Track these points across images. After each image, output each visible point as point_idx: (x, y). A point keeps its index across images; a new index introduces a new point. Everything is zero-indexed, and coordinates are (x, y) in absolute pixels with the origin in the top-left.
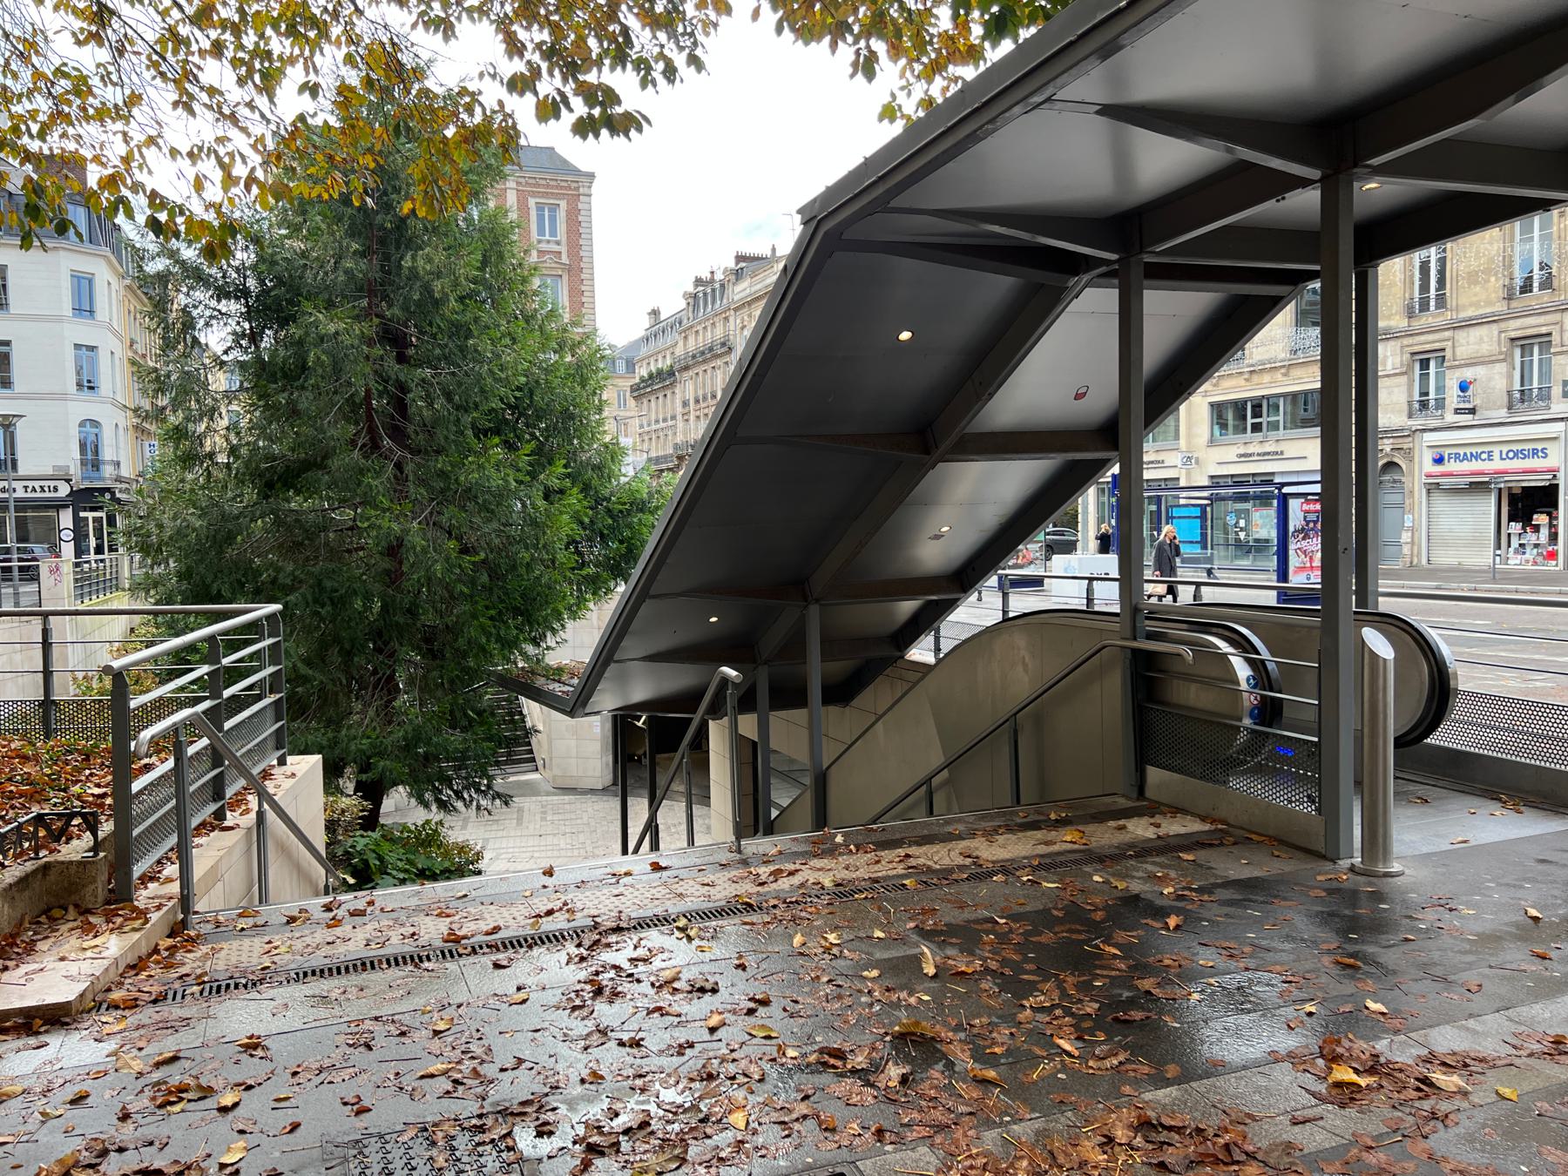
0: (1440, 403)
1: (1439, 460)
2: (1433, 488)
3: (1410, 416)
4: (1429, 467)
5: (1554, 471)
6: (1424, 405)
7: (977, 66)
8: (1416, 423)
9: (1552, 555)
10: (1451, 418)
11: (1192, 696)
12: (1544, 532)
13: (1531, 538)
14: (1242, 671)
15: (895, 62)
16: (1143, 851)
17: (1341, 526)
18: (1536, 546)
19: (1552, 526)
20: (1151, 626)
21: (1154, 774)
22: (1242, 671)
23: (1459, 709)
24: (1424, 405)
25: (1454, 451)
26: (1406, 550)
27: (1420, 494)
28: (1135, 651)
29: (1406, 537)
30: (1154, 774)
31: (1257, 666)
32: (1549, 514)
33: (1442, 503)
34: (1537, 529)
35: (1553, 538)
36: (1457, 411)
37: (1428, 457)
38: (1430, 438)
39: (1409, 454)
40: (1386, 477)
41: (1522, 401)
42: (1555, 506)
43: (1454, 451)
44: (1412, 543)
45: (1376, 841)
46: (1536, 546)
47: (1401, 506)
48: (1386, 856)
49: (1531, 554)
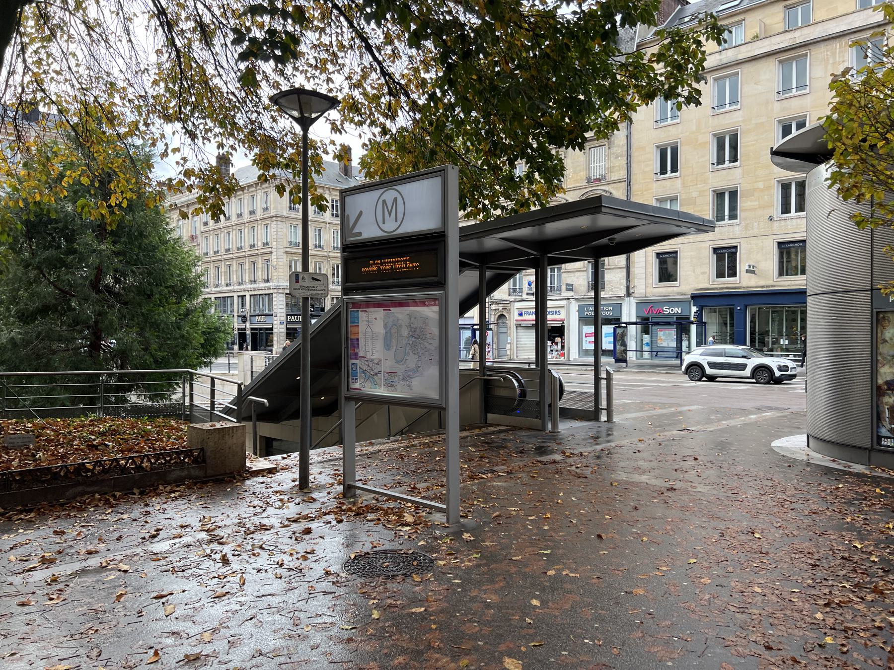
0: (521, 290)
1: (521, 315)
2: (518, 326)
3: (509, 295)
4: (517, 317)
5: (563, 320)
6: (514, 290)
7: (464, 211)
8: (512, 298)
9: (563, 355)
10: (525, 297)
11: (503, 393)
12: (560, 345)
13: (555, 347)
14: (516, 384)
15: (341, 145)
16: (493, 433)
17: (734, 351)
18: (557, 351)
19: (562, 343)
20: (488, 373)
21: (489, 415)
22: (516, 384)
23: (565, 396)
24: (514, 290)
25: (526, 310)
26: (508, 352)
27: (514, 328)
28: (485, 379)
29: (508, 347)
30: (489, 415)
31: (519, 381)
32: (561, 338)
33: (521, 331)
34: (557, 344)
35: (563, 347)
36: (527, 294)
37: (516, 313)
38: (517, 305)
39: (509, 311)
40: (500, 321)
41: (551, 291)
42: (563, 335)
43: (526, 310)
44: (511, 349)
45: (555, 426)
46: (557, 351)
47: (506, 333)
48: (557, 428)
49: (555, 354)
